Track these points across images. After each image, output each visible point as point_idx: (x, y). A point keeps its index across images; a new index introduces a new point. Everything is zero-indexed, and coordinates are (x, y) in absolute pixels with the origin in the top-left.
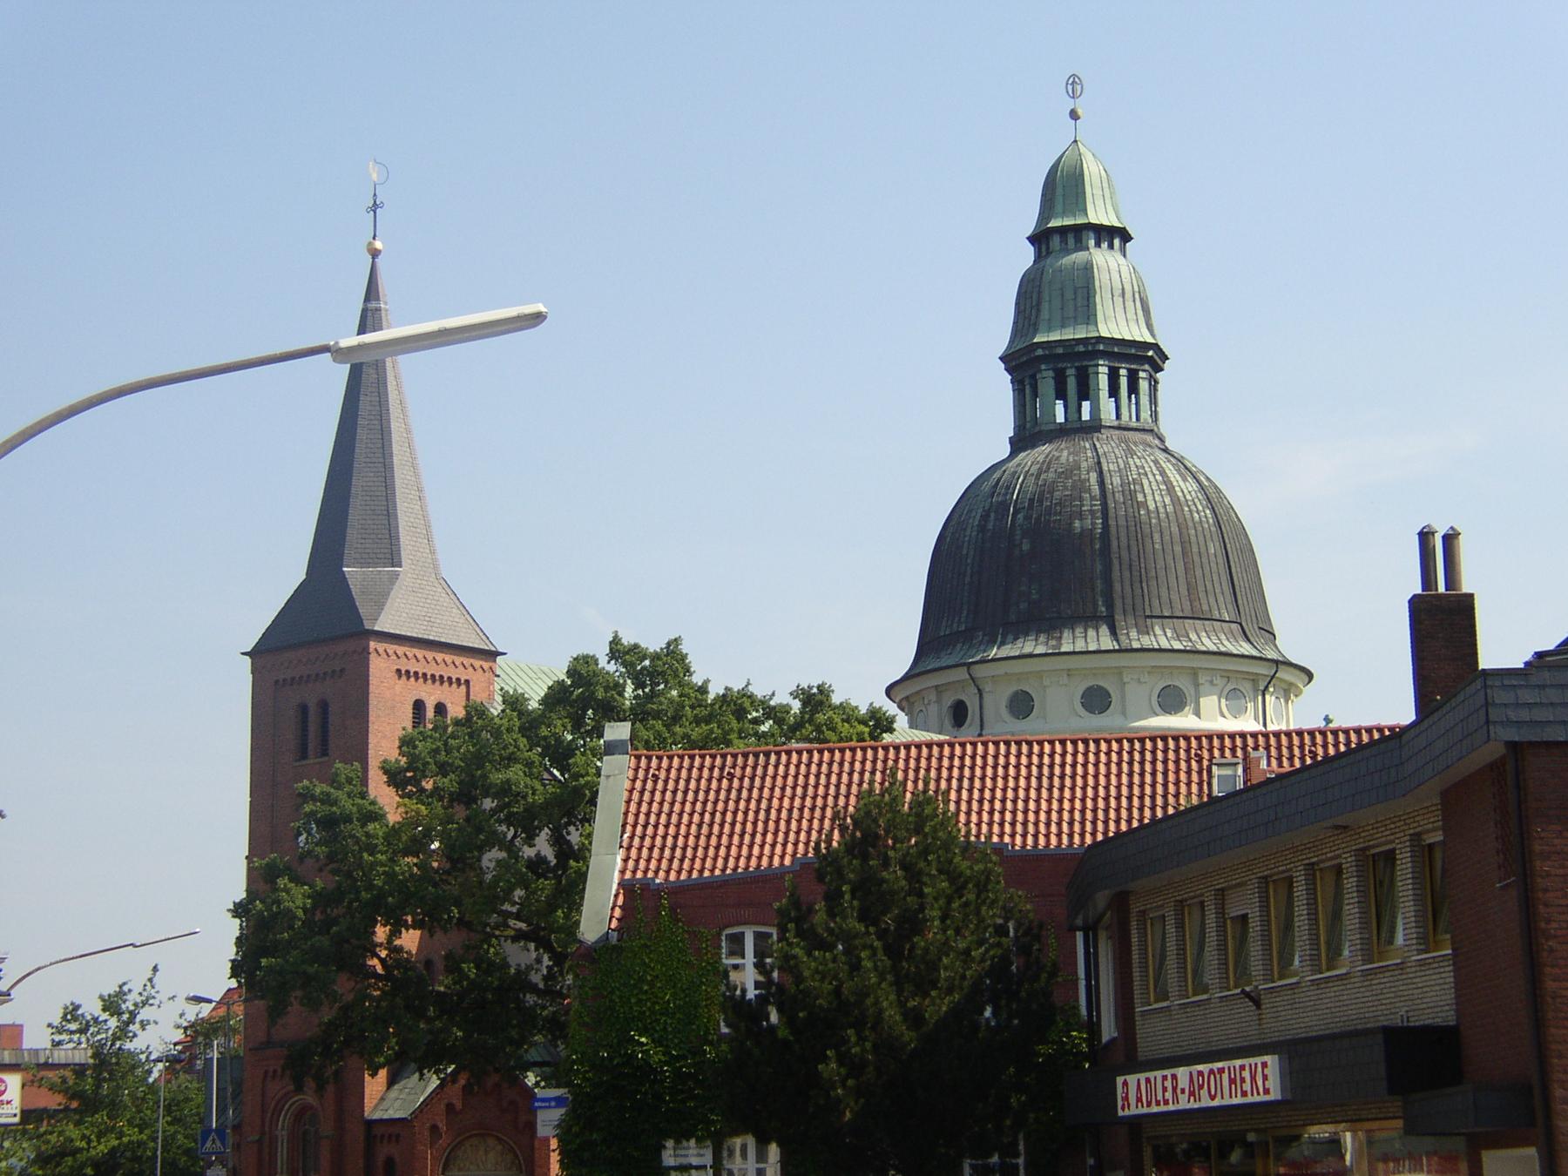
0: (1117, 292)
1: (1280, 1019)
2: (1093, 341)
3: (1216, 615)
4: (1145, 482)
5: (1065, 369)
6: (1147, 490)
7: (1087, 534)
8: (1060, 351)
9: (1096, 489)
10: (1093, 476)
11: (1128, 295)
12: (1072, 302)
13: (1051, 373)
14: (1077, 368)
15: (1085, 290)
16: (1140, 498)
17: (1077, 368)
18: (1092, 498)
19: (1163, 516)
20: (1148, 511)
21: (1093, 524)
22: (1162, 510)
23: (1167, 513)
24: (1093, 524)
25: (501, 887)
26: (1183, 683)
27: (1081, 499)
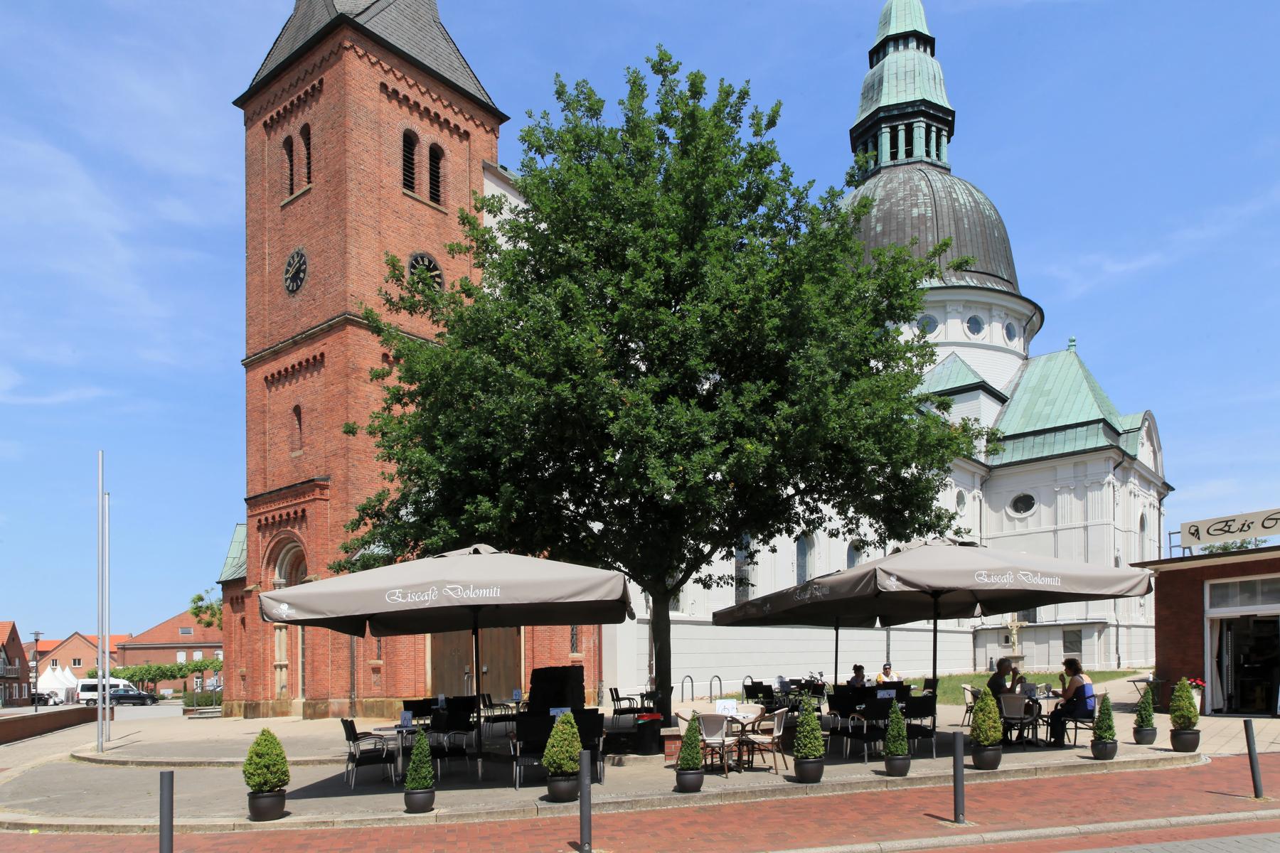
0: (932, 77)
2: (918, 103)
3: (1000, 275)
4: (956, 187)
5: (897, 126)
6: (958, 192)
7: (922, 217)
8: (896, 112)
9: (926, 190)
10: (923, 183)
11: (937, 80)
13: (888, 130)
14: (906, 125)
16: (954, 196)
17: (906, 125)
18: (924, 195)
19: (969, 208)
20: (960, 204)
21: (926, 210)
22: (968, 204)
26: (982, 315)
27: (917, 196)
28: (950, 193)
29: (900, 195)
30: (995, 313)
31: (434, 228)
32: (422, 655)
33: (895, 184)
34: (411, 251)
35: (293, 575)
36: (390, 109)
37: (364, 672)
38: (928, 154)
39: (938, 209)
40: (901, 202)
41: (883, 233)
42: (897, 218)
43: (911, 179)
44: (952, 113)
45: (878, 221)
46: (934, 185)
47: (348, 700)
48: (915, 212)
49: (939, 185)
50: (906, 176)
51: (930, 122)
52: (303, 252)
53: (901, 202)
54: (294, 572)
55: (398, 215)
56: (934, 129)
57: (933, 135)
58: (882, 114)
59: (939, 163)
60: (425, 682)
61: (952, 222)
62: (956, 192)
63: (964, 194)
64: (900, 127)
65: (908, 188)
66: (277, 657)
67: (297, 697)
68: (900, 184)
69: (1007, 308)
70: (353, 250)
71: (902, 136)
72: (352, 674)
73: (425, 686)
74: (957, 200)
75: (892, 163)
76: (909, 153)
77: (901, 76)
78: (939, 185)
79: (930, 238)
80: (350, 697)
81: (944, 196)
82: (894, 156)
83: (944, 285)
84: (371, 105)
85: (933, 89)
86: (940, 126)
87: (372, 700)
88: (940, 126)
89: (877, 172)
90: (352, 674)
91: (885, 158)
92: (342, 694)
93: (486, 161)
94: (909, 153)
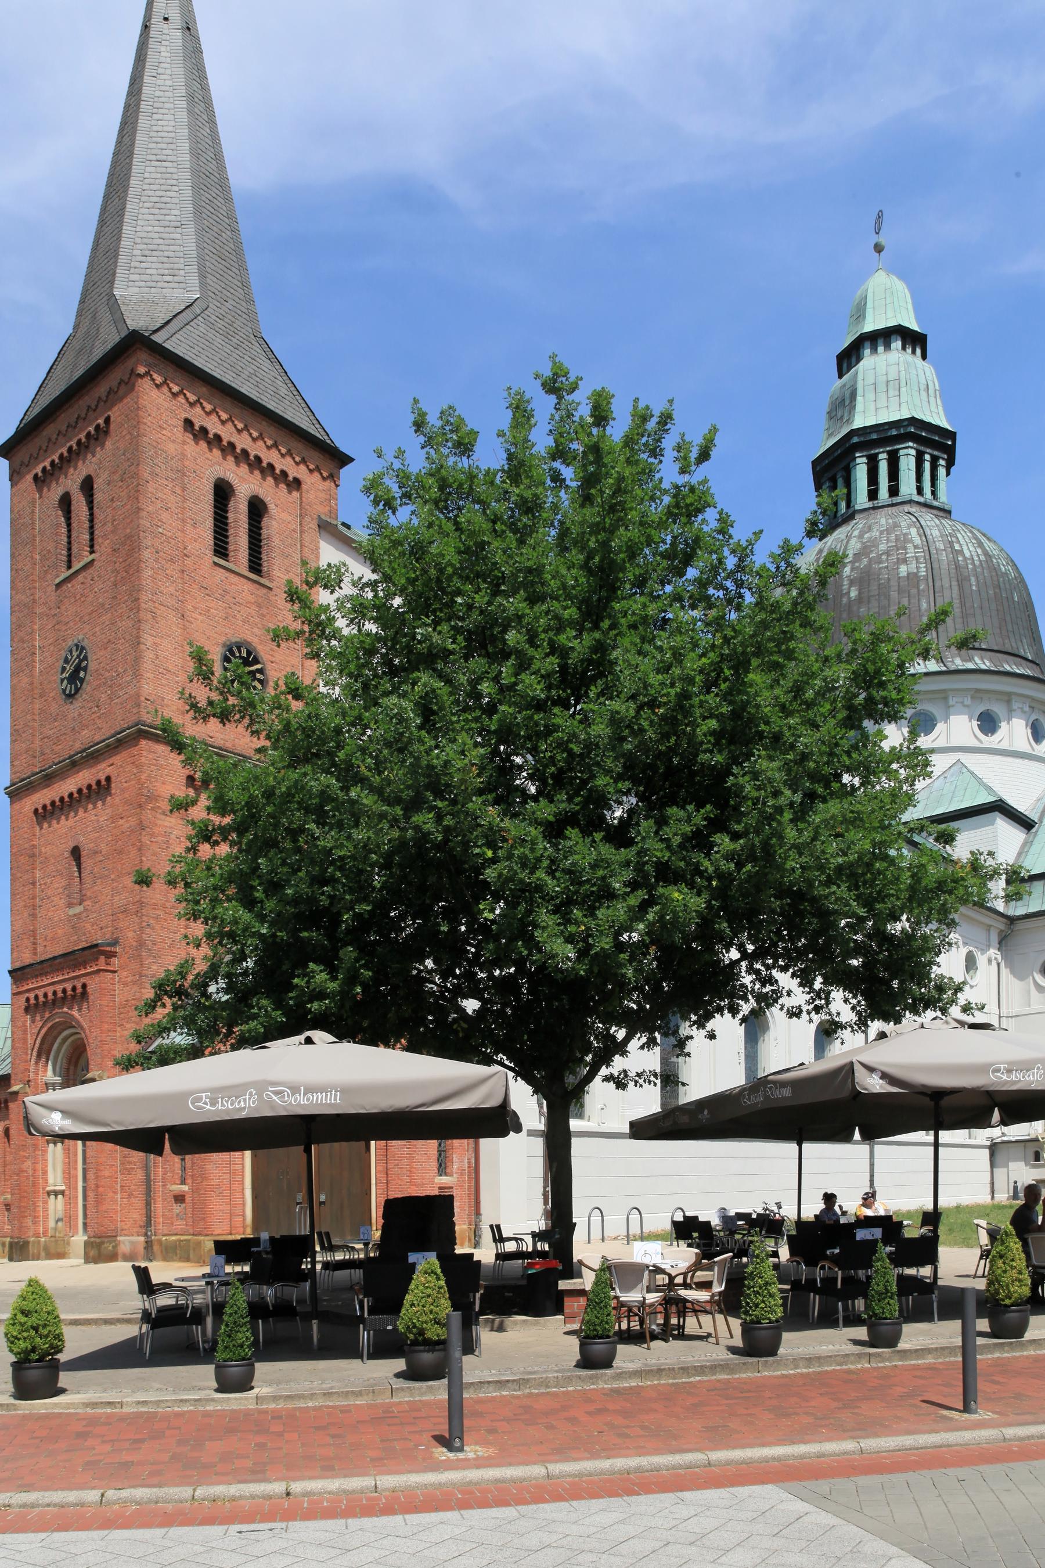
0: (923, 387)
1: (223, 285)
2: (906, 423)
3: (1022, 653)
4: (959, 536)
5: (877, 455)
7: (912, 577)
9: (917, 541)
10: (914, 531)
11: (931, 392)
12: (884, 395)
13: (865, 460)
15: (897, 382)
16: (957, 547)
17: (888, 452)
18: (916, 547)
19: (977, 563)
20: (965, 559)
21: (918, 568)
22: (976, 558)
23: (980, 561)
24: (918, 568)
25: (510, 889)
27: (905, 548)
28: (951, 543)
29: (882, 547)
30: (1015, 705)
31: (254, 607)
32: (239, 1178)
33: (875, 533)
34: (224, 639)
35: (71, 1072)
36: (196, 451)
37: (164, 1200)
38: (920, 491)
39: (935, 566)
40: (884, 557)
41: (860, 599)
42: (879, 579)
43: (896, 525)
44: (952, 435)
45: (852, 583)
46: (928, 532)
47: (142, 1239)
48: (903, 570)
49: (936, 533)
50: (890, 521)
51: (922, 448)
52: (83, 644)
53: (884, 557)
54: (72, 1068)
55: (207, 592)
56: (927, 457)
57: (927, 466)
58: (856, 440)
59: (935, 503)
60: (244, 1215)
61: (954, 583)
62: (958, 542)
63: (970, 545)
64: (881, 456)
65: (893, 537)
66: (51, 1180)
67: (77, 1233)
68: (881, 533)
69: (1033, 699)
70: (148, 640)
71: (883, 467)
72: (148, 1204)
73: (244, 1220)
74: (961, 552)
75: (870, 504)
76: (894, 491)
77: (882, 387)
78: (936, 533)
79: (924, 606)
80: (146, 1235)
81: (942, 547)
82: (873, 495)
83: (944, 669)
84: (172, 448)
85: (925, 404)
86: (936, 453)
87: (174, 1238)
88: (936, 453)
89: (850, 517)
90: (148, 1204)
91: (861, 498)
92: (135, 1230)
93: (323, 517)
94: (894, 491)
